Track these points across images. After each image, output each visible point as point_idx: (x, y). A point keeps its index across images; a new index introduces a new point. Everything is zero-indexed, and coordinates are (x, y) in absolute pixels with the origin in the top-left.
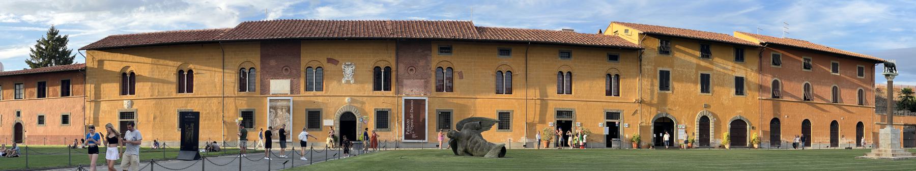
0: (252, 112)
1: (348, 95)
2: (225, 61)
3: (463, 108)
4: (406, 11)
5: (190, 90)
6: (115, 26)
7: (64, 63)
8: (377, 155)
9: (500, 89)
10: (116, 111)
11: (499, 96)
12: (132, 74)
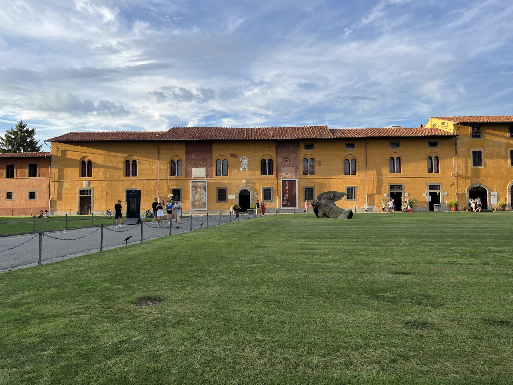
0: (180, 190)
1: (245, 178)
2: (160, 154)
3: (321, 185)
4: (280, 121)
5: (134, 174)
6: (75, 125)
7: (32, 151)
8: (264, 218)
9: (347, 172)
10: (76, 189)
11: (347, 176)
12: (90, 162)
